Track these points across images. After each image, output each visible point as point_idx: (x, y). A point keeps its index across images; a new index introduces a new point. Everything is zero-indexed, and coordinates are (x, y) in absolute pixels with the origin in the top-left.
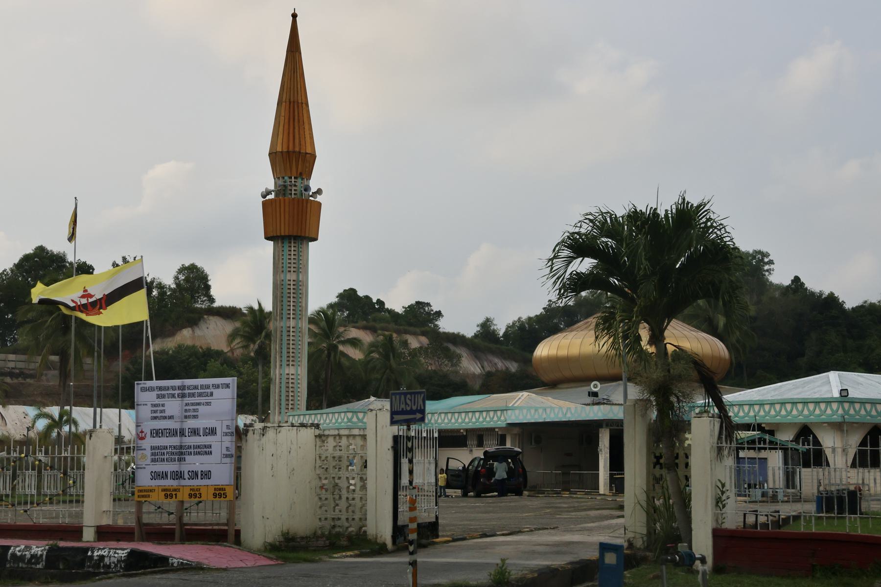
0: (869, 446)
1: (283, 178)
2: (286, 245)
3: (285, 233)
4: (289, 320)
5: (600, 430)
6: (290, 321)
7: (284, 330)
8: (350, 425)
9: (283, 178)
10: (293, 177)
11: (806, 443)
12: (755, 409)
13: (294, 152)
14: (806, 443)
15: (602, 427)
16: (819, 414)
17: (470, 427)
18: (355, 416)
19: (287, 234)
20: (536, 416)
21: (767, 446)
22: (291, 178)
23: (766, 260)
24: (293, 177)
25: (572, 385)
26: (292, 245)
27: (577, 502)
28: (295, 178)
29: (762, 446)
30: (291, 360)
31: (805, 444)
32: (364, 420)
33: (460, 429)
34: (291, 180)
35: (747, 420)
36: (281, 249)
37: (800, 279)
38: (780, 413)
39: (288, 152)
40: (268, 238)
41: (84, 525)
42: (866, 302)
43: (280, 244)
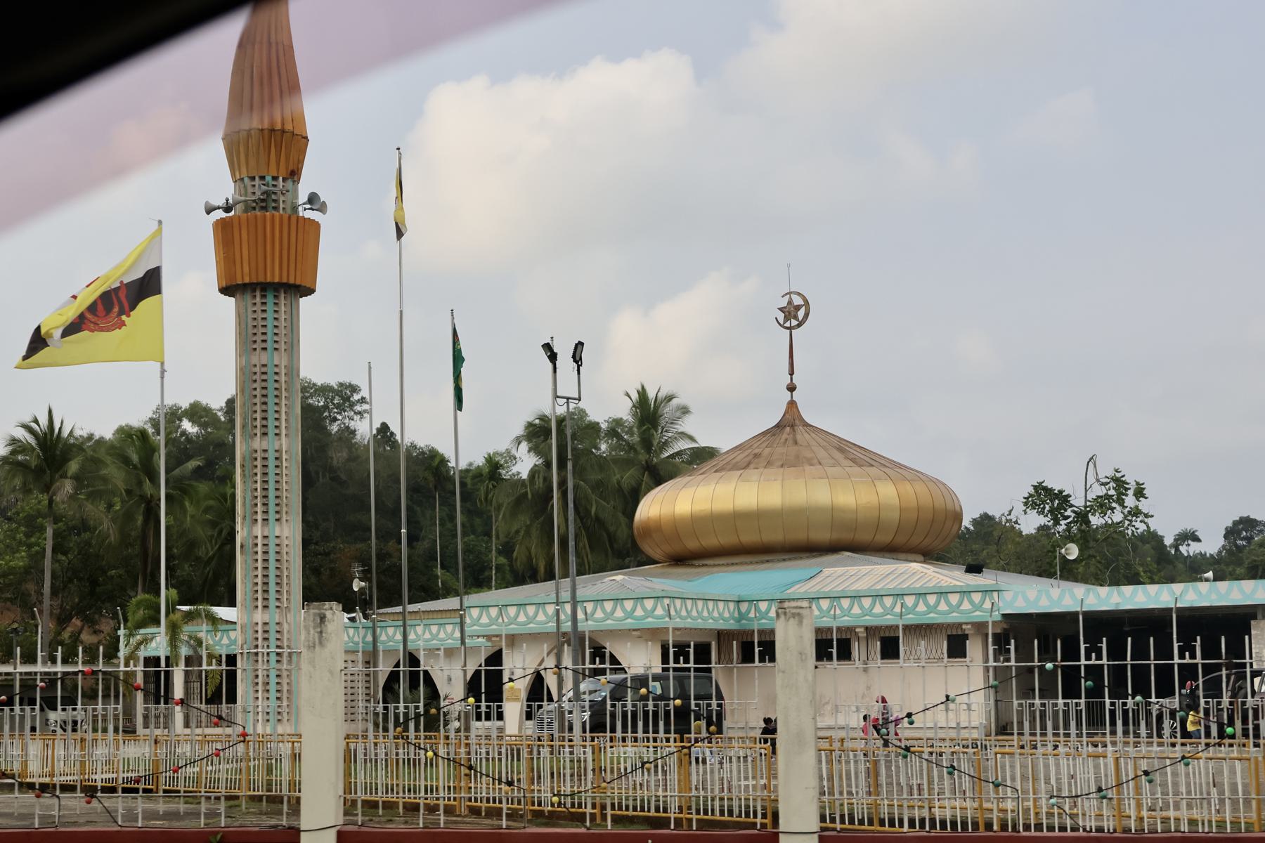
0: (1036, 660)
1: (262, 178)
2: (270, 300)
3: (257, 278)
4: (277, 438)
5: (1253, 622)
6: (280, 439)
7: (271, 455)
8: (514, 628)
9: (262, 178)
10: (281, 179)
11: (682, 658)
12: (491, 614)
13: (272, 130)
14: (682, 658)
15: (1255, 618)
16: (602, 618)
17: (847, 624)
18: (639, 606)
19: (247, 280)
20: (1214, 597)
21: (607, 665)
22: (275, 178)
23: (356, 397)
24: (281, 179)
25: (803, 555)
26: (282, 301)
27: (59, 761)
28: (284, 180)
29: (598, 666)
30: (268, 509)
31: (1091, 656)
32: (649, 609)
33: (855, 627)
34: (253, 183)
35: (630, 623)
36: (258, 308)
37: (388, 428)
38: (767, 614)
39: (272, 130)
40: (226, 290)
41: (780, 830)
42: (471, 464)
43: (258, 300)
